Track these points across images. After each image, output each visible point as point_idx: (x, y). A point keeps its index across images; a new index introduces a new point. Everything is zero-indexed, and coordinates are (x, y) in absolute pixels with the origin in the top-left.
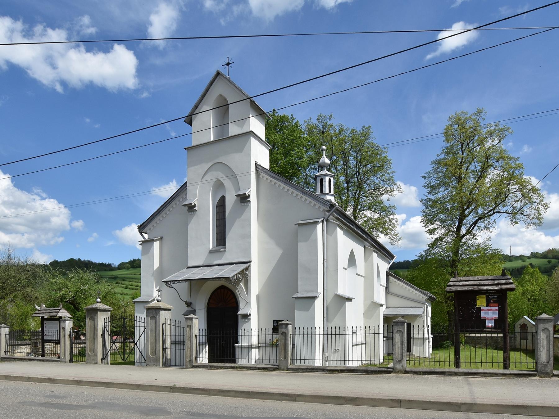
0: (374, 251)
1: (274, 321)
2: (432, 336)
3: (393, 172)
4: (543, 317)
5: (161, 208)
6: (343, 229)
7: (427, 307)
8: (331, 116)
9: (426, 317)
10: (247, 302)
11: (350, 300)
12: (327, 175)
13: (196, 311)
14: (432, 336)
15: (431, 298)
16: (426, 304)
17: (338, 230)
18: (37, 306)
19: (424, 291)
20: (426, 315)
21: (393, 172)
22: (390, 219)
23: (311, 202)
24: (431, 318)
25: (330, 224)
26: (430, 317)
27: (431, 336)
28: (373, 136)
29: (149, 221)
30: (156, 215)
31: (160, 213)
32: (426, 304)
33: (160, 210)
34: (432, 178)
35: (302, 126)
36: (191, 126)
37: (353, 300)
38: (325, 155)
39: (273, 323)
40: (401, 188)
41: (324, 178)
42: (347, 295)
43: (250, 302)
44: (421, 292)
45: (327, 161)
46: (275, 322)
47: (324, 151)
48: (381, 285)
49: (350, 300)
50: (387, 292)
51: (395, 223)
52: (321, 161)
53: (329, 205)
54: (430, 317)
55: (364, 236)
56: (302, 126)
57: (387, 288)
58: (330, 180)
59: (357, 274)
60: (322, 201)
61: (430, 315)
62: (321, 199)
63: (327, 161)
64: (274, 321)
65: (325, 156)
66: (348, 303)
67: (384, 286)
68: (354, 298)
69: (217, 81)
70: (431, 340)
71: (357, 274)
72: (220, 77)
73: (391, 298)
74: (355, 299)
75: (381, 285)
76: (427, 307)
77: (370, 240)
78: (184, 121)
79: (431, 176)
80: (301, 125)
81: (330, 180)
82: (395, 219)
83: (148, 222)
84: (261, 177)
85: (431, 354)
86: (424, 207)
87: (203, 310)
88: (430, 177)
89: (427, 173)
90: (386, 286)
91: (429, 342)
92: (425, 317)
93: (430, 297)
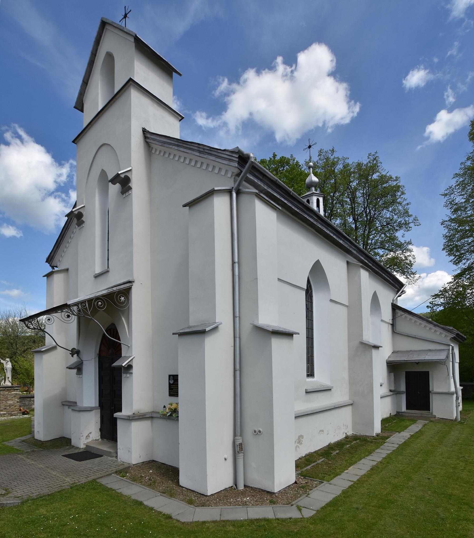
0: (362, 267)
1: (170, 376)
2: (462, 388)
3: (408, 204)
4: (115, 365)
5: (64, 231)
6: (276, 209)
7: (453, 349)
8: (333, 150)
9: (451, 363)
10: (129, 347)
11: (376, 347)
12: (314, 194)
13: (84, 361)
14: (462, 388)
15: (458, 337)
16: (452, 344)
17: (256, 204)
18: (2, 360)
19: (448, 327)
20: (451, 361)
21: (408, 204)
22: (406, 257)
23: (417, 322)
24: (460, 363)
25: (244, 198)
26: (90, 410)
27: (460, 388)
28: (382, 168)
29: (54, 250)
30: (61, 241)
31: (63, 238)
32: (451, 346)
33: (63, 233)
34: (455, 194)
35: (303, 165)
36: (83, 112)
37: (294, 335)
38: (313, 173)
39: (169, 380)
40: (418, 220)
41: (311, 199)
42: (372, 341)
43: (131, 346)
44: (443, 328)
45: (315, 179)
46: (171, 377)
47: (311, 168)
48: (382, 321)
49: (376, 347)
50: (394, 331)
51: (412, 260)
52: (307, 180)
53: (237, 160)
54: (90, 410)
55: (341, 242)
56: (303, 165)
57: (393, 325)
58: (318, 201)
59: (331, 301)
60: (227, 157)
61: (457, 359)
62: (224, 153)
63: (315, 179)
64: (170, 376)
65: (312, 175)
66: (374, 351)
67: (389, 323)
68: (382, 346)
69: (105, 33)
70: (460, 393)
71: (331, 301)
72: (106, 28)
73: (399, 338)
74: (298, 334)
75: (382, 321)
76: (453, 349)
77: (355, 252)
78: (74, 107)
79: (454, 192)
80: (302, 165)
81: (318, 201)
82: (411, 256)
83: (54, 251)
84: (154, 152)
85: (460, 411)
86: (447, 230)
87: (93, 360)
88: (452, 194)
89: (448, 189)
90: (391, 322)
91: (457, 398)
92: (450, 364)
93: (457, 335)
